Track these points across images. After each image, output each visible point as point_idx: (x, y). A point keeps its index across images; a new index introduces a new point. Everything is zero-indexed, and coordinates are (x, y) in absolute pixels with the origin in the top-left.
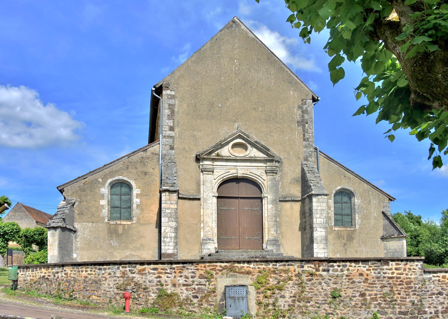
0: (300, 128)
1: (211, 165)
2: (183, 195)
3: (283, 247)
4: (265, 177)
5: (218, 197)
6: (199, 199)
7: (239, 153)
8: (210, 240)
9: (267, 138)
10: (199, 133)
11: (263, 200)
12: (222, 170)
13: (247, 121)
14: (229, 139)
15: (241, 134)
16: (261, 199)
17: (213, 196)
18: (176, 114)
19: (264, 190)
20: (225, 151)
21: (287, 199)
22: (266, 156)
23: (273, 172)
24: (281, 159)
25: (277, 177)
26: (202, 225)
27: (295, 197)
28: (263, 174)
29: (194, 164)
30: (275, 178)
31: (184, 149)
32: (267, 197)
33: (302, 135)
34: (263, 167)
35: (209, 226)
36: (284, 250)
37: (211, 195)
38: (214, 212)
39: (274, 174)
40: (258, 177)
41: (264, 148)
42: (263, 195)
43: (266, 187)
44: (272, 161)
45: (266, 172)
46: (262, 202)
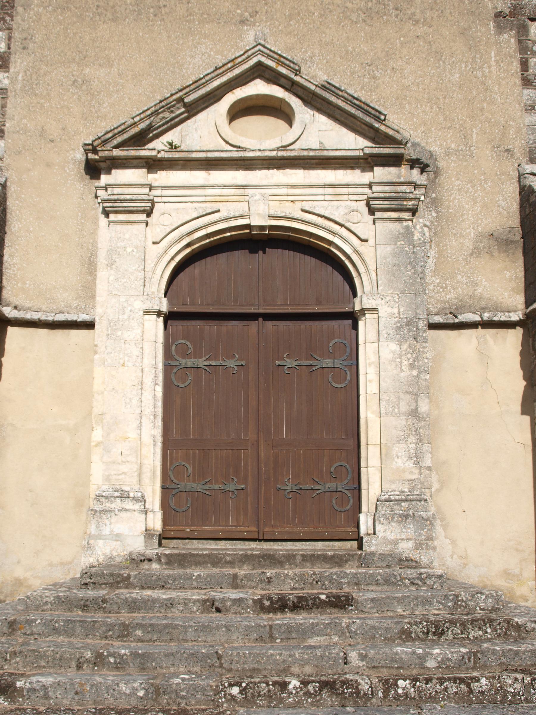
0: (509, 39)
1: (142, 185)
2: (27, 310)
3: (445, 527)
4: (364, 224)
5: (170, 318)
6: (89, 325)
7: (261, 135)
8: (124, 496)
9: (374, 78)
10: (102, 72)
11: (361, 324)
12: (191, 205)
13: (290, 17)
14: (216, 83)
15: (263, 59)
16: (353, 318)
17: (147, 312)
18: (20, 9)
19: (364, 283)
20: (205, 132)
21: (462, 318)
22: (370, 144)
23: (402, 206)
24: (431, 154)
25: (420, 226)
26: (98, 435)
27: (496, 309)
28: (356, 217)
29: (78, 185)
30: (408, 233)
31: (42, 134)
32: (374, 310)
33: (516, 66)
34: (357, 185)
35: (126, 439)
36: (454, 542)
37: (139, 305)
38: (148, 380)
39: (406, 215)
40: (336, 228)
41: (358, 108)
42: (357, 301)
43: (372, 266)
44: (395, 161)
45: (368, 205)
46: (355, 327)
